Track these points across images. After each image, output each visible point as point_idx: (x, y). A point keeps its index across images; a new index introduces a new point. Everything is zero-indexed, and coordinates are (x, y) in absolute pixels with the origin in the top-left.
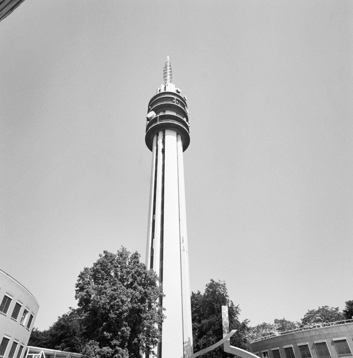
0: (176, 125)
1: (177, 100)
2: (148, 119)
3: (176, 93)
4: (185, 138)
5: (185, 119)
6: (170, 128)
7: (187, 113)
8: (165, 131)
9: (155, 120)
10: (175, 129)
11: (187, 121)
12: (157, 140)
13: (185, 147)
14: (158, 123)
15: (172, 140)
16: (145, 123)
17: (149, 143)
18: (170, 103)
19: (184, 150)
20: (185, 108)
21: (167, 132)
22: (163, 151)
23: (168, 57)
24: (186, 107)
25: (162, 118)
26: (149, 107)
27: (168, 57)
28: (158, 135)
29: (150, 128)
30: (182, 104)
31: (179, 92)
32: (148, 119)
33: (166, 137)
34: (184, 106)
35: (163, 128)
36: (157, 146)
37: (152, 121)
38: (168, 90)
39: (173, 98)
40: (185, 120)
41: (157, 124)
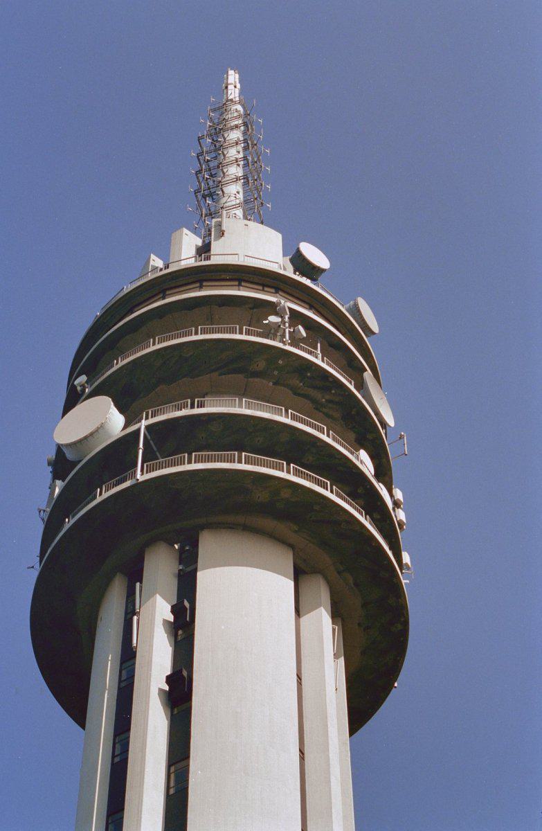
0: (285, 494)
1: (296, 317)
2: (61, 463)
3: (289, 272)
4: (365, 605)
5: (363, 454)
6: (240, 519)
7: (384, 425)
8: (195, 545)
9: (118, 456)
10: (282, 528)
11: (383, 472)
12: (130, 612)
13: (367, 694)
14: (140, 477)
15: (257, 624)
16: (44, 489)
17: (65, 652)
18: (244, 337)
19: (359, 715)
20: (361, 385)
21: (208, 544)
22: (179, 693)
23: (233, 77)
24: (368, 375)
25: (169, 440)
26: (73, 375)
27: (233, 77)
28: (135, 574)
29: (69, 523)
30: (333, 348)
31: (312, 271)
32: (61, 463)
33: (206, 579)
34: (354, 370)
35: (186, 520)
36: (128, 655)
37: (78, 471)
38: (225, 252)
39: (272, 308)
40: (364, 462)
41: (127, 484)
